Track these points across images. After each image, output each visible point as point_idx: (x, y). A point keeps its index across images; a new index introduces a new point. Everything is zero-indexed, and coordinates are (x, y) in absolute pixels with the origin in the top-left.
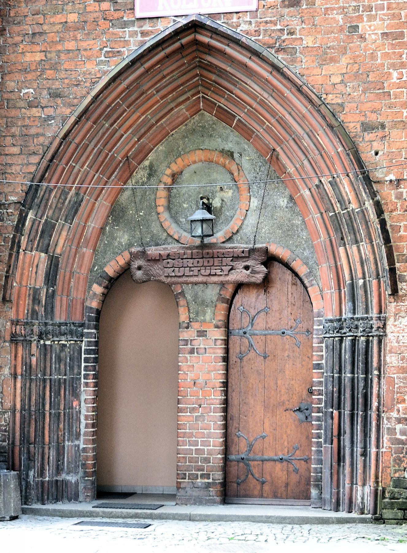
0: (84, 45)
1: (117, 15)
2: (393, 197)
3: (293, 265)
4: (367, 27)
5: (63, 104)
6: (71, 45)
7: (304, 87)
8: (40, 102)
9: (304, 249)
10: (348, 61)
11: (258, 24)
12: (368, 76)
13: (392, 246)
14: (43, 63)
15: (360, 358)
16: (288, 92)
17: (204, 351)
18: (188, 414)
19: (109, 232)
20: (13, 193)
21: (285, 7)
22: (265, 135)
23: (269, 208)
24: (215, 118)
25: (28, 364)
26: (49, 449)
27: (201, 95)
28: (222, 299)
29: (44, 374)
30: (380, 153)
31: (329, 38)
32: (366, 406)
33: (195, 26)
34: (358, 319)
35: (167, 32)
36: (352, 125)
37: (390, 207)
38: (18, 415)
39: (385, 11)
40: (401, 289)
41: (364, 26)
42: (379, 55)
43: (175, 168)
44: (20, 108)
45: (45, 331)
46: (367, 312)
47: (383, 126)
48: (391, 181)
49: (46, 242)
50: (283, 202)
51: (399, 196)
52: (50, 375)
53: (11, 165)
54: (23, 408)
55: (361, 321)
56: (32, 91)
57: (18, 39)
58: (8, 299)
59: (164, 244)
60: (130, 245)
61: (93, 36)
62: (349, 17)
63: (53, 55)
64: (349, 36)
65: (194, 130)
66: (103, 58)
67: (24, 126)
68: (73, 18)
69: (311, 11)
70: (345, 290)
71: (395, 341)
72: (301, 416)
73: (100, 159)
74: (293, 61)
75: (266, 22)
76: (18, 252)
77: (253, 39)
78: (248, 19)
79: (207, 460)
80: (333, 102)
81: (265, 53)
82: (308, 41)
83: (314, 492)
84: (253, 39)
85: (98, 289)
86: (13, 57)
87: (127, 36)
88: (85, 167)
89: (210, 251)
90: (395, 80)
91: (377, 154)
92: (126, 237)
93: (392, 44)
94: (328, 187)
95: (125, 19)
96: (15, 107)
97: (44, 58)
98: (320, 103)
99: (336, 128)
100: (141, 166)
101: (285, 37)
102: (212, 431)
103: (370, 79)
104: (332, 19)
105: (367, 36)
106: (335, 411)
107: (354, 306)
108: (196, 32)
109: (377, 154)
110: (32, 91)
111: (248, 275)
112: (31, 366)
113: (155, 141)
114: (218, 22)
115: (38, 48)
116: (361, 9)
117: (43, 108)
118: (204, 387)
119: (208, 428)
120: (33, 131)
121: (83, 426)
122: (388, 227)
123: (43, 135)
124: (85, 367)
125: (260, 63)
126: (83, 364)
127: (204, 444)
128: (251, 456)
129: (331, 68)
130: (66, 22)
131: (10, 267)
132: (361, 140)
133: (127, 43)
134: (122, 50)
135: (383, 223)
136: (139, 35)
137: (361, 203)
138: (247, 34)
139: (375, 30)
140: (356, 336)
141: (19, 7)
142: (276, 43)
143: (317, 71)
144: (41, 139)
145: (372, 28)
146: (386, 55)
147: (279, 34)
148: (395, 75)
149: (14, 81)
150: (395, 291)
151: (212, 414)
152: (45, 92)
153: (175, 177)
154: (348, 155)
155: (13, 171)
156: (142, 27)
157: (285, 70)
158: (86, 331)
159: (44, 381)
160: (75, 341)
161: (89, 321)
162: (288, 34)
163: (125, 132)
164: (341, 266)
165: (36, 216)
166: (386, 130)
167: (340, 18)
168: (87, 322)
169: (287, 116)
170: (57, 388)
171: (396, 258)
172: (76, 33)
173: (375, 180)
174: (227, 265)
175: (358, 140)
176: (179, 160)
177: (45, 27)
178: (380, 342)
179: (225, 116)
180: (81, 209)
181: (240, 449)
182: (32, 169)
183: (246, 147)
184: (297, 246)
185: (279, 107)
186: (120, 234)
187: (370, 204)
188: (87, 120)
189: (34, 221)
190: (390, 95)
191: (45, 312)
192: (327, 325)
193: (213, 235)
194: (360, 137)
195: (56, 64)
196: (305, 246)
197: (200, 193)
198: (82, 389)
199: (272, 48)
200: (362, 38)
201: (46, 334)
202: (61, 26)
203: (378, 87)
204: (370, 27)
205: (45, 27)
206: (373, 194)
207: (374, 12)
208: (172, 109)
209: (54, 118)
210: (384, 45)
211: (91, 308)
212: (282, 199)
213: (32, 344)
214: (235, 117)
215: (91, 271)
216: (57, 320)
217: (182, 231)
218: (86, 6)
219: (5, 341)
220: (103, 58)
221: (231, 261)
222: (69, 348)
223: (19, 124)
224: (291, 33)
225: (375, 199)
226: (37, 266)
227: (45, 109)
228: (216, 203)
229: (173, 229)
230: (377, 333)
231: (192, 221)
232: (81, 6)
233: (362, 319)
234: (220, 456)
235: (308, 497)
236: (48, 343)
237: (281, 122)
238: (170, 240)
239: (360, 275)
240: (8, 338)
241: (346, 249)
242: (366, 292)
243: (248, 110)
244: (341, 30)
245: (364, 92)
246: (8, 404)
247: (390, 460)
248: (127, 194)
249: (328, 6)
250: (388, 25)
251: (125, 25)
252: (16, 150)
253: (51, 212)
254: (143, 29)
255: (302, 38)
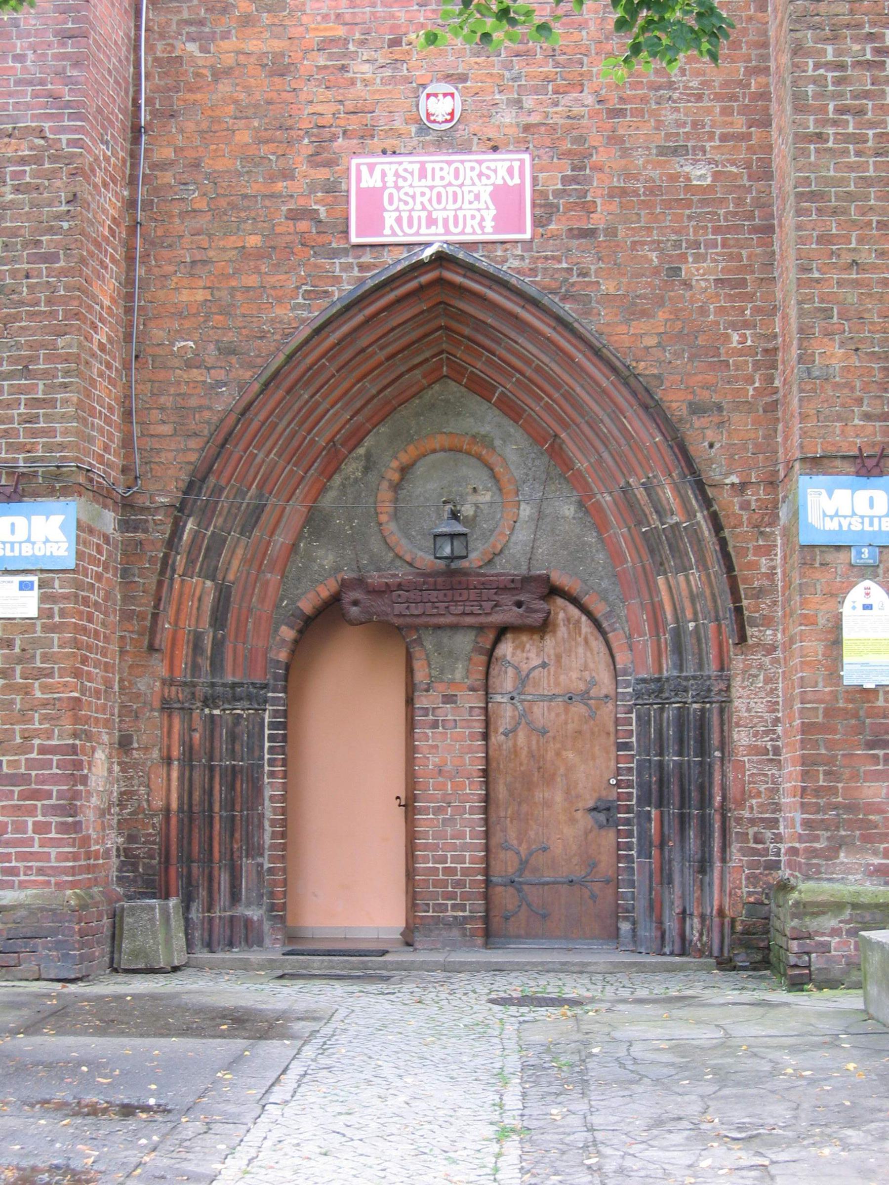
0: (272, 280)
1: (321, 239)
2: (737, 507)
3: (585, 600)
4: (693, 270)
5: (238, 363)
6: (252, 280)
7: (605, 350)
8: (204, 361)
9: (602, 578)
10: (667, 316)
11: (534, 260)
12: (696, 338)
13: (735, 576)
14: (208, 304)
15: (692, 734)
16: (580, 356)
17: (453, 724)
18: (431, 816)
19: (305, 550)
20: (162, 492)
21: (572, 238)
22: (544, 414)
23: (548, 520)
24: (463, 389)
25: (187, 743)
26: (220, 868)
27: (444, 356)
28: (478, 650)
29: (211, 759)
30: (717, 446)
31: (638, 283)
32: (705, 800)
33: (441, 259)
34: (687, 679)
35: (399, 268)
36: (674, 405)
37: (733, 521)
38: (174, 821)
39: (719, 250)
40: (752, 636)
41: (690, 269)
42: (712, 310)
43: (404, 458)
44: (173, 368)
45: (212, 696)
46: (701, 666)
47: (720, 409)
48: (733, 484)
49: (214, 563)
50: (569, 510)
51: (745, 506)
52: (221, 760)
53: (158, 451)
54: (180, 809)
55: (692, 682)
56: (191, 344)
57: (171, 269)
58: (157, 647)
59: (389, 568)
60: (337, 569)
61: (286, 268)
62: (667, 255)
63: (224, 294)
64: (667, 281)
65: (433, 405)
66: (300, 300)
67: (179, 395)
68: (254, 241)
69: (612, 244)
70: (666, 638)
71: (744, 710)
72: (602, 817)
73: (295, 443)
74: (587, 313)
75: (546, 258)
76: (172, 579)
77: (527, 280)
78: (519, 252)
79: (459, 884)
80: (647, 372)
81: (545, 301)
82: (608, 286)
83: (625, 927)
84: (527, 280)
85: (287, 633)
86: (161, 294)
87: (338, 269)
88: (272, 456)
89: (464, 578)
90: (735, 344)
91: (711, 446)
92: (331, 557)
93: (730, 295)
94: (641, 494)
95: (334, 245)
96: (165, 368)
97: (210, 298)
98: (628, 373)
99: (653, 409)
100: (354, 455)
101: (574, 279)
102: (468, 840)
103: (700, 342)
104: (642, 256)
105: (694, 283)
106: (653, 811)
107: (681, 660)
108: (441, 266)
109: (711, 446)
110: (191, 344)
111: (522, 615)
112: (191, 748)
113: (375, 420)
114: (475, 255)
115: (201, 283)
116: (684, 245)
117: (208, 369)
118: (455, 777)
119: (461, 835)
120: (193, 402)
121: (267, 836)
122: (730, 549)
123: (210, 408)
124: (270, 748)
125: (538, 314)
126: (267, 745)
127: (454, 859)
128: (528, 877)
129: (640, 326)
130: (243, 247)
131: (160, 600)
132: (688, 426)
133: (337, 280)
134: (330, 289)
135: (723, 543)
136: (356, 269)
137: (690, 514)
138: (518, 273)
139: (703, 275)
140: (685, 703)
141: (170, 223)
142: (560, 288)
143: (622, 329)
144: (207, 415)
145: (701, 271)
146: (721, 310)
147: (564, 274)
148: (735, 337)
149: (164, 330)
150: (742, 638)
151: (467, 816)
152: (212, 346)
153: (405, 470)
154: (671, 447)
155: (162, 460)
156: (360, 257)
157: (576, 325)
158: (270, 695)
159: (212, 769)
160: (256, 710)
161: (276, 680)
162: (578, 276)
163: (332, 406)
164: (661, 603)
165: (198, 525)
166: (725, 413)
167: (654, 256)
168: (271, 682)
169: (578, 389)
170: (229, 779)
171: (742, 592)
172: (259, 262)
173: (710, 483)
174: (489, 600)
175: (685, 428)
176: (411, 448)
177: (211, 253)
178: (722, 711)
179: (481, 388)
180: (264, 517)
181: (506, 864)
182: (193, 457)
183: (512, 430)
184: (590, 575)
185: (566, 377)
186: (321, 553)
187: (704, 517)
188: (278, 387)
189: (196, 535)
190: (728, 365)
191: (211, 665)
192: (639, 687)
193: (466, 557)
194: (686, 423)
195: (229, 306)
196: (603, 573)
197: (441, 495)
198: (266, 780)
199: (555, 294)
200: (687, 285)
201: (214, 700)
202: (234, 252)
203: (711, 354)
204: (698, 270)
205: (211, 253)
206: (707, 502)
207: (702, 250)
208: (401, 376)
209: (225, 384)
210: (718, 295)
211: (278, 661)
212: (567, 507)
213: (194, 715)
214: (496, 388)
215: (277, 606)
216: (230, 679)
217: (416, 550)
218: (274, 225)
219: (152, 710)
220: (300, 300)
221: (496, 593)
222: (247, 719)
223: (172, 391)
224: (583, 274)
225: (712, 509)
226: (200, 600)
227: (212, 371)
228: (467, 510)
229: (405, 547)
230: (718, 698)
231: (436, 536)
232: (265, 225)
233: (694, 678)
234: (479, 877)
235: (615, 935)
236: (217, 712)
237: (569, 397)
238: (398, 563)
239: (689, 615)
240: (157, 704)
241: (667, 579)
242: (699, 640)
243: (517, 380)
244: (656, 272)
245: (691, 358)
246: (158, 803)
247: (741, 879)
248: (331, 495)
249: (636, 239)
250: (723, 268)
251: (335, 254)
252: (166, 429)
253: (220, 520)
254: (362, 260)
255: (598, 282)
